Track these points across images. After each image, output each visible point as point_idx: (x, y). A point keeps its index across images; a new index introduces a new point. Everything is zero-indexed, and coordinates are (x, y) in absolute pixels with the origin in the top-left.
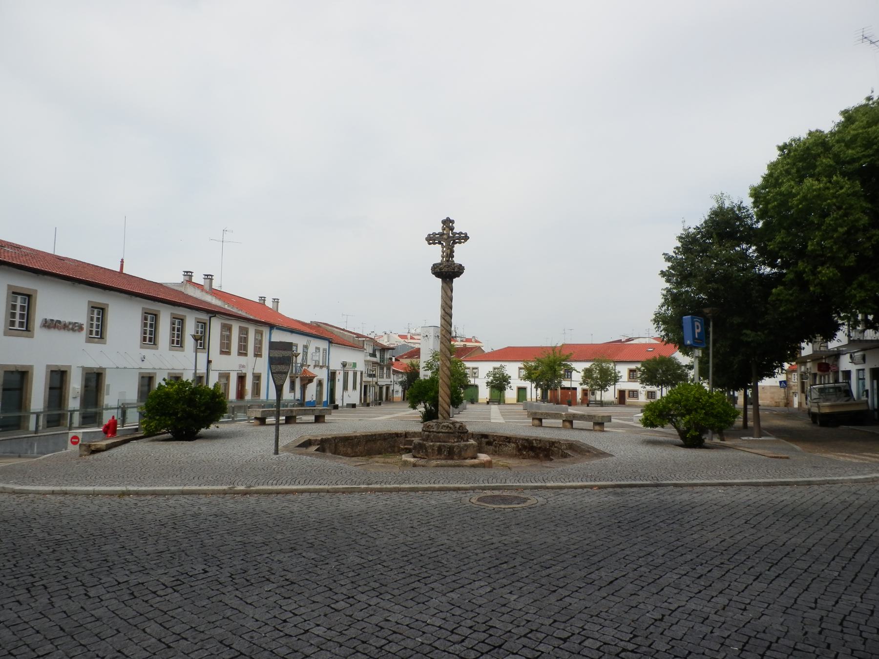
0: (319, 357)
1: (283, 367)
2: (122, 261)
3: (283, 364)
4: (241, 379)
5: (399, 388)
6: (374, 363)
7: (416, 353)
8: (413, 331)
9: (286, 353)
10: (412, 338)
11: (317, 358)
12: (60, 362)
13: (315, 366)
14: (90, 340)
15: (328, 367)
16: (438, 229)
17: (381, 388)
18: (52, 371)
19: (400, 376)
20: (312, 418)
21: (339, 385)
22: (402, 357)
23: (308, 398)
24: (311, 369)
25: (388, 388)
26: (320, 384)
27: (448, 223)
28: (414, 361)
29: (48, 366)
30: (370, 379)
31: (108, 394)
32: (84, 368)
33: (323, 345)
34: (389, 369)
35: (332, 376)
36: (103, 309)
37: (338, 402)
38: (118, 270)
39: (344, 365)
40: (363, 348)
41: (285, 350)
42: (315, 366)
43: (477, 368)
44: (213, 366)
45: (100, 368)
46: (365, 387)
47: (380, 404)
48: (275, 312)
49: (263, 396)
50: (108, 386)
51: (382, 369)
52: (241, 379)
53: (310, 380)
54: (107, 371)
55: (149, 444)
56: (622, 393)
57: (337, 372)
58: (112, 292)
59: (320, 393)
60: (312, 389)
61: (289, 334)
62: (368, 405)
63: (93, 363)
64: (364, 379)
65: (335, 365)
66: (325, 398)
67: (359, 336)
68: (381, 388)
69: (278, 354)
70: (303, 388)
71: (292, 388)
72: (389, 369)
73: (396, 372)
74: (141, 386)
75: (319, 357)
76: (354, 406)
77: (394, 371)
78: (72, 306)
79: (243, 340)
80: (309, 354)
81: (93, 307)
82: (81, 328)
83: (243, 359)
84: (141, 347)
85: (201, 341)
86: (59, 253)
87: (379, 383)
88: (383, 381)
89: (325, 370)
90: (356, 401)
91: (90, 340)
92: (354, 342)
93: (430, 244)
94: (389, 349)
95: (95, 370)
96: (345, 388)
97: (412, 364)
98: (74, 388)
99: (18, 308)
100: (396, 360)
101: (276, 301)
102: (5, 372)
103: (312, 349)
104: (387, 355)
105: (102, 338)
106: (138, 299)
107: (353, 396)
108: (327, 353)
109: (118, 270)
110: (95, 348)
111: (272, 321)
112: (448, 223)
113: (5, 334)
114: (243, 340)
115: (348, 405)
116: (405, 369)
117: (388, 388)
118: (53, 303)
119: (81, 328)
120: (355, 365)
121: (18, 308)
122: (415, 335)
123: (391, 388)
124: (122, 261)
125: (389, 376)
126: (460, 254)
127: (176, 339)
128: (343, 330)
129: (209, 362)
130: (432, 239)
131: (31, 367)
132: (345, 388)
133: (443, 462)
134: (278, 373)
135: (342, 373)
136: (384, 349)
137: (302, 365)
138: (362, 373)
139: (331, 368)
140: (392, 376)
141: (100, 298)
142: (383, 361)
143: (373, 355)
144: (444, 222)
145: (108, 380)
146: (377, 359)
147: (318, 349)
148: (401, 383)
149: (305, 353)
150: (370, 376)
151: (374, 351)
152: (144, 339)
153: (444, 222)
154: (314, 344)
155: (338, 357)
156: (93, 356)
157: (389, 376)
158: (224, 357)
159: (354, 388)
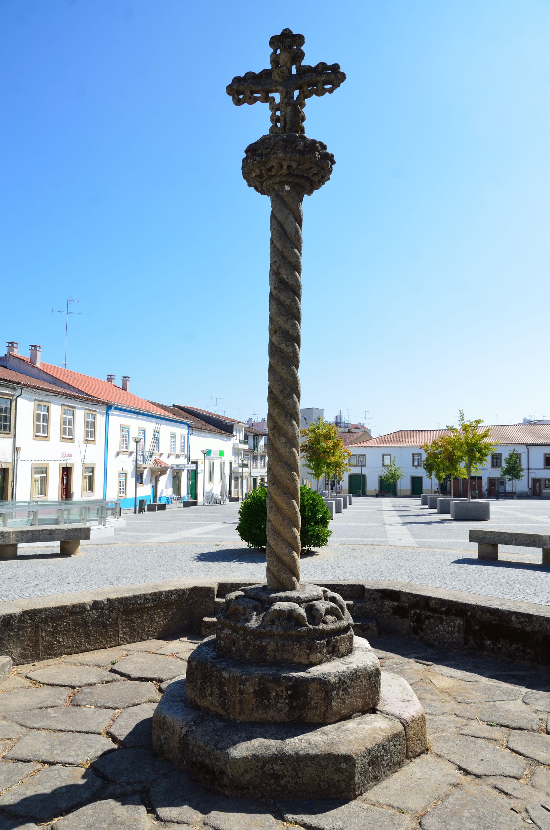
4: (67, 472)
16: (260, 60)
17: (255, 480)
24: (164, 459)
27: (288, 44)
43: (364, 455)
44: (21, 455)
52: (67, 472)
56: (536, 481)
70: (155, 481)
79: (90, 426)
83: (67, 447)
85: (67, 434)
93: (238, 102)
96: (211, 479)
112: (288, 44)
114: (90, 426)
120: (221, 453)
126: (320, 118)
129: (16, 450)
130: (244, 89)
144: (275, 41)
153: (275, 41)
158: (40, 443)
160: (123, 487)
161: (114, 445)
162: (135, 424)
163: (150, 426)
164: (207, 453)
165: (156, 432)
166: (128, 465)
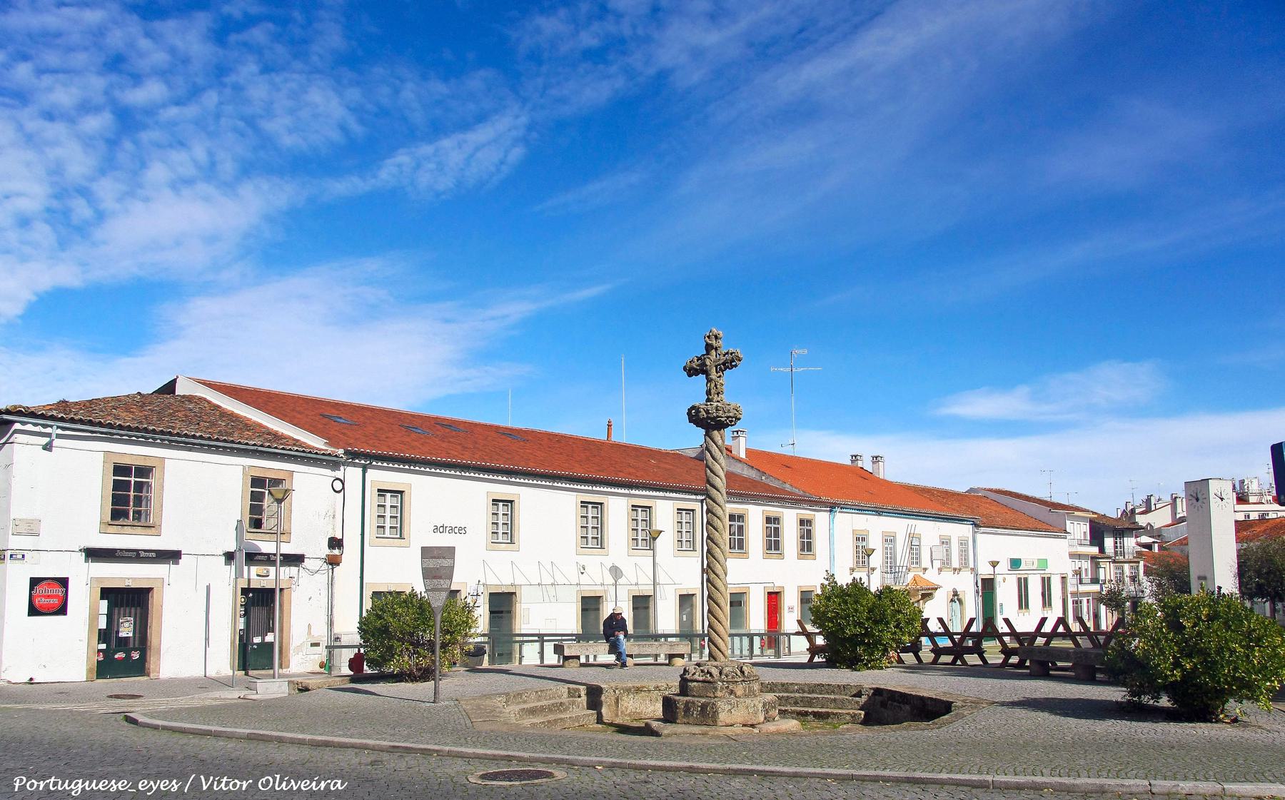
33: (961, 531)
35: (988, 587)
64: (1070, 589)
158: (774, 563)
163: (899, 526)
164: (1015, 563)
165: (889, 539)
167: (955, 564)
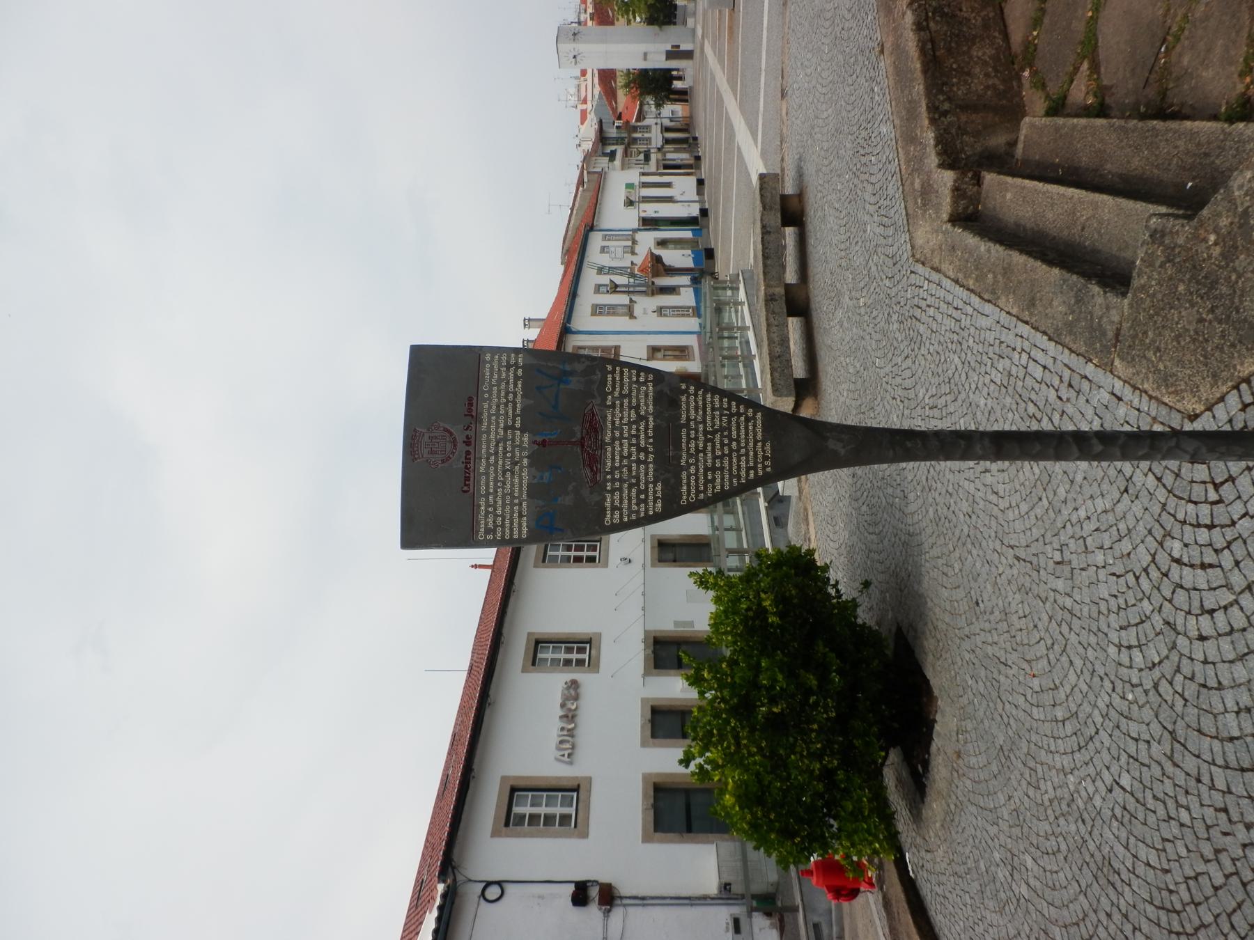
0: (617, 246)
1: (616, 417)
2: (476, 566)
3: (594, 428)
5: (667, 109)
6: (626, 154)
7: (606, 77)
8: (573, 100)
9: (501, 406)
10: (585, 101)
11: (620, 250)
12: (635, 721)
13: (633, 253)
14: (592, 665)
15: (635, 231)
17: (667, 141)
18: (653, 736)
19: (646, 108)
20: (790, 232)
21: (666, 211)
22: (614, 110)
23: (689, 263)
24: (639, 260)
25: (668, 129)
26: (662, 243)
28: (620, 81)
29: (644, 744)
30: (653, 157)
31: (691, 624)
32: (647, 673)
33: (596, 240)
34: (635, 129)
35: (650, 223)
36: (538, 642)
37: (694, 211)
38: (489, 571)
39: (630, 203)
40: (600, 174)
41: (472, 415)
42: (633, 253)
45: (645, 641)
46: (666, 167)
47: (695, 139)
48: (546, 323)
49: (691, 341)
50: (676, 623)
51: (635, 140)
53: (658, 260)
54: (650, 627)
55: (934, 830)
57: (643, 215)
58: (505, 631)
59: (679, 243)
60: (674, 257)
61: (577, 300)
62: (698, 158)
63: (634, 653)
65: (630, 219)
66: (687, 234)
67: (581, 182)
68: (667, 141)
69: (506, 475)
70: (672, 271)
71: (671, 290)
72: (635, 129)
73: (641, 116)
74: (675, 561)
75: (617, 246)
76: (700, 182)
77: (638, 120)
78: (533, 697)
80: (614, 264)
81: (534, 661)
82: (574, 684)
84: (606, 565)
86: (467, 667)
87: (660, 144)
88: (656, 138)
89: (640, 236)
90: (691, 182)
91: (592, 665)
92: (591, 190)
94: (601, 130)
95: (650, 651)
96: (669, 200)
97: (627, 86)
98: (683, 690)
99: (569, 656)
100: (619, 118)
101: (528, 323)
102: (656, 830)
103: (605, 260)
104: (612, 132)
105: (589, 642)
106: (516, 580)
107: (684, 186)
108: (610, 234)
109: (489, 571)
110: (608, 654)
111: (557, 331)
113: (584, 835)
115: (700, 192)
116: (634, 98)
117: (668, 129)
118: (527, 745)
119: (574, 684)
121: (569, 656)
122: (579, 97)
123: (667, 123)
124: (476, 566)
125: (647, 128)
127: (573, 553)
128: (572, 210)
131: (646, 777)
132: (669, 200)
133: (525, 481)
134: (668, 468)
135: (644, 206)
136: (602, 138)
137: (632, 275)
138: (643, 174)
139: (635, 225)
140: (646, 122)
141: (517, 650)
142: (623, 139)
143: (612, 156)
145: (666, 625)
146: (620, 150)
147: (603, 250)
148: (658, 106)
149: (612, 270)
150: (647, 158)
151: (605, 155)
152: (591, 560)
154: (595, 256)
155: (617, 215)
156: (624, 654)
157: (647, 128)
159: (668, 185)
160: (680, 311)
161: (621, 323)
162: (587, 297)
164: (630, 203)
165: (601, 270)
166: (646, 305)
167: (629, 243)
